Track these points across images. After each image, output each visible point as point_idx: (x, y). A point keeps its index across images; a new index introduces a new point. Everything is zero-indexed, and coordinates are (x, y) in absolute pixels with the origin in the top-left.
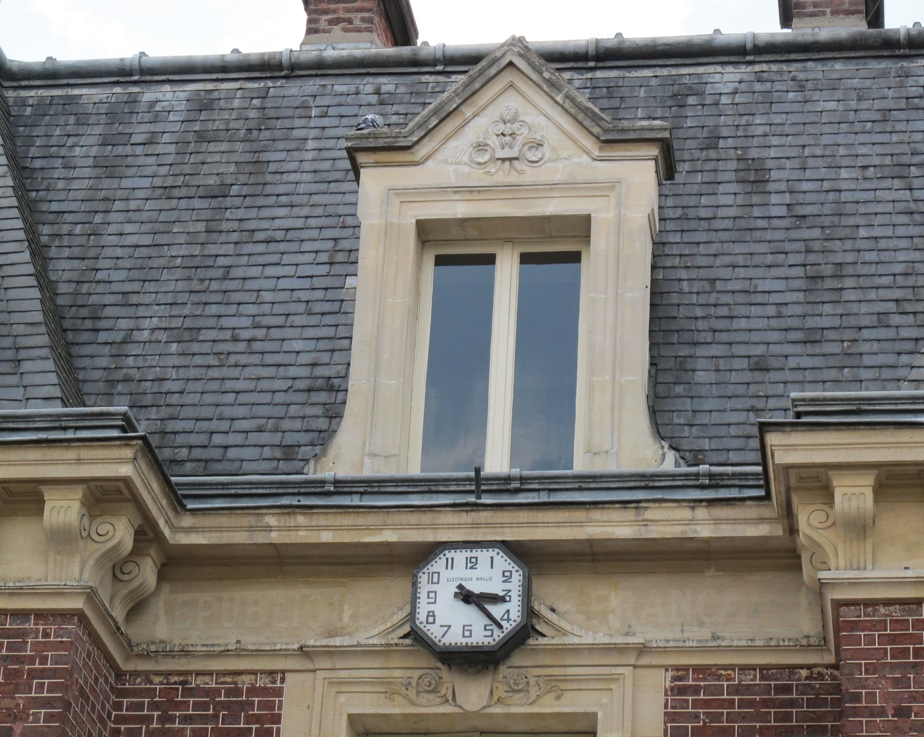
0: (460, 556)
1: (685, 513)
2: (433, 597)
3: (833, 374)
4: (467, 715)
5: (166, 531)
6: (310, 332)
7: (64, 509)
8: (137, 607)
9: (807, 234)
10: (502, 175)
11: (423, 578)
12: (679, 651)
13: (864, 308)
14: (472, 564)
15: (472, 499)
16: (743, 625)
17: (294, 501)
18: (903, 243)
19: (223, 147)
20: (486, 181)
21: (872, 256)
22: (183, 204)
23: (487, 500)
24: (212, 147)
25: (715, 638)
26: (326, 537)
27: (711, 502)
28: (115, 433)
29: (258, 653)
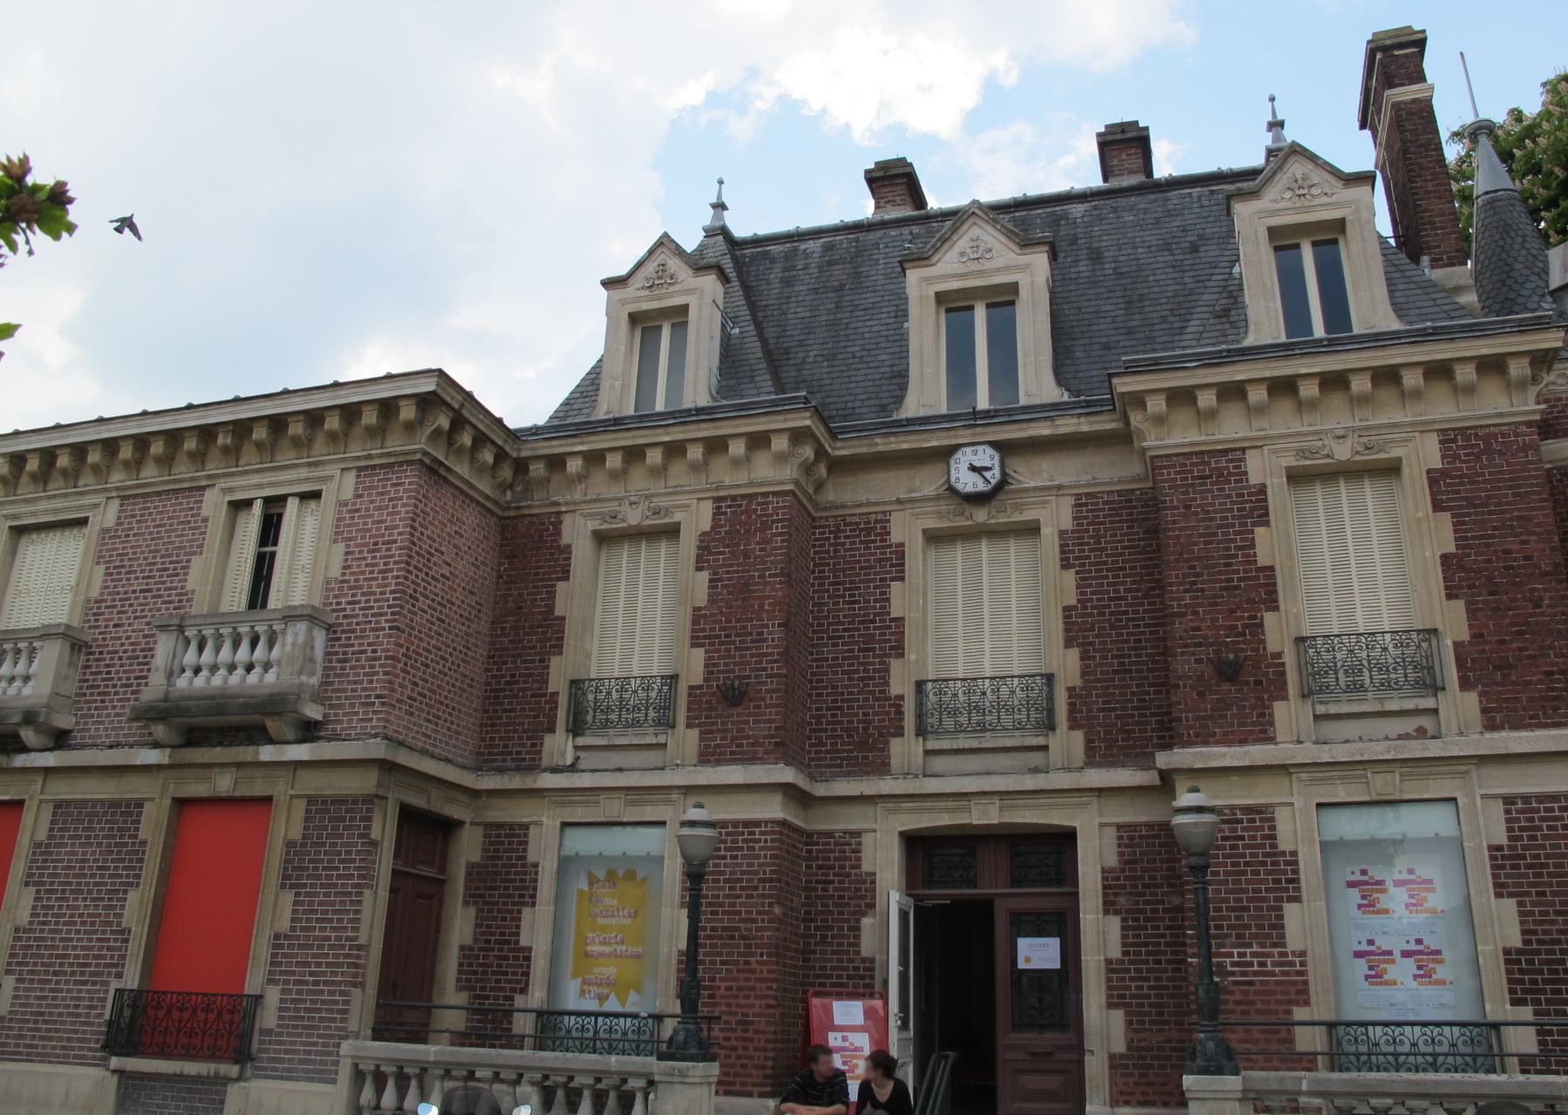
0: (969, 450)
4: (978, 525)
7: (780, 444)
8: (819, 486)
10: (974, 267)
20: (966, 270)
26: (905, 446)
27: (1087, 414)
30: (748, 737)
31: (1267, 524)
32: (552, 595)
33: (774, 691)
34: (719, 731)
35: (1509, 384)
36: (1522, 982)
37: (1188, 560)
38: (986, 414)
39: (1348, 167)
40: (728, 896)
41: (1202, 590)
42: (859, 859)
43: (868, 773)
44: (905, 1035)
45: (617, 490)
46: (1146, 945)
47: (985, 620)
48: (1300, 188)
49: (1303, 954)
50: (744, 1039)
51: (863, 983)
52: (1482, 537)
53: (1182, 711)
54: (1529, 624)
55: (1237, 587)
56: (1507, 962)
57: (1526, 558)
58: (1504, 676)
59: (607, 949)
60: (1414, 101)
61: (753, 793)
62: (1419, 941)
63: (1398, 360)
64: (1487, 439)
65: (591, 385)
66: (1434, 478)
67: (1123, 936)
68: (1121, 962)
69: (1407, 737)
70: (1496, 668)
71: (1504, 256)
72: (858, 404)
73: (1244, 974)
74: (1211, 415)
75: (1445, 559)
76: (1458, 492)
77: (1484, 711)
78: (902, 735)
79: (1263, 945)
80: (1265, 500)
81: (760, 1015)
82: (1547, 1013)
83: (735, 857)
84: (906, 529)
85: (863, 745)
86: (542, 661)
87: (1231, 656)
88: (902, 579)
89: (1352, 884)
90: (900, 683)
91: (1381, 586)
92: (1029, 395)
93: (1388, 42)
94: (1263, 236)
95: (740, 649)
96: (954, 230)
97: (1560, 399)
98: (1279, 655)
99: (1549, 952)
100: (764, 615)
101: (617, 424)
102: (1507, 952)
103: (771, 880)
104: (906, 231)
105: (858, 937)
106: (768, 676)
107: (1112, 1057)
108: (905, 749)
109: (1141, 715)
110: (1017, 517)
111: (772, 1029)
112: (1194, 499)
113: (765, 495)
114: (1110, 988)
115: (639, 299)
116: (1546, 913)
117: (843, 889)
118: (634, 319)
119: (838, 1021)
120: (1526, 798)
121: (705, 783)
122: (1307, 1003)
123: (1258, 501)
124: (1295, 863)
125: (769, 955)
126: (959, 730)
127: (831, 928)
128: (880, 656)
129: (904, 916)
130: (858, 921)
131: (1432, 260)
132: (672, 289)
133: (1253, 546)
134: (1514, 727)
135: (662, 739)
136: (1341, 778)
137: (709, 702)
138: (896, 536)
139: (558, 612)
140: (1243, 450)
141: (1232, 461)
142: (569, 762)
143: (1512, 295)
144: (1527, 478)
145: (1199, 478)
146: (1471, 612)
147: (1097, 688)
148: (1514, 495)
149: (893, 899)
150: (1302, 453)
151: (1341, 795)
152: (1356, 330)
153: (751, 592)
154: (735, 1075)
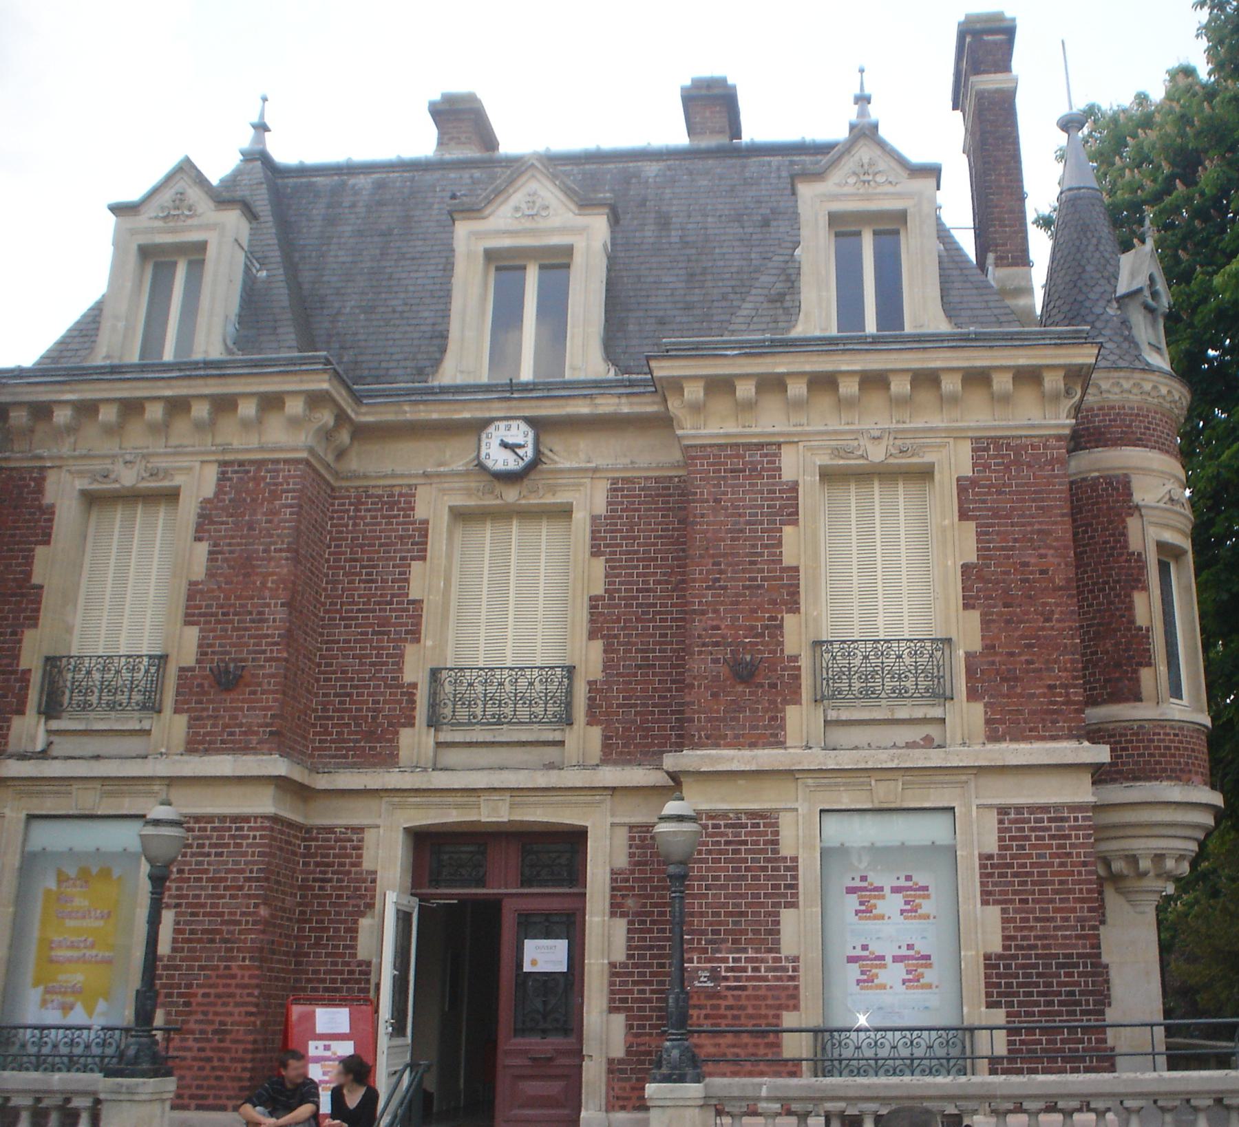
0: (502, 425)
1: (616, 400)
2: (488, 445)
3: (697, 326)
4: (508, 504)
5: (353, 416)
6: (433, 307)
7: (295, 407)
8: (341, 454)
9: (688, 252)
10: (528, 224)
11: (484, 436)
12: (613, 470)
13: (716, 291)
14: (509, 428)
15: (508, 395)
16: (643, 457)
17: (419, 398)
18: (737, 256)
19: (391, 208)
20: (520, 227)
21: (722, 263)
22: (369, 239)
23: (515, 396)
24: (385, 208)
25: (632, 463)
26: (435, 416)
27: (628, 395)
28: (320, 367)
29: (402, 476)
30: (241, 725)
31: (795, 523)
32: (29, 560)
33: (272, 676)
34: (209, 717)
35: (1043, 396)
36: (999, 985)
37: (713, 556)
38: (525, 387)
39: (916, 157)
40: (211, 897)
41: (725, 588)
42: (360, 856)
43: (374, 765)
44: (399, 1041)
45: (109, 446)
46: (651, 948)
47: (509, 608)
48: (865, 173)
49: (796, 959)
50: (220, 1050)
51: (353, 988)
52: (1003, 549)
53: (695, 712)
54: (1038, 638)
55: (759, 587)
56: (987, 967)
57: (1042, 572)
58: (1009, 688)
59: (74, 954)
60: (997, 91)
61: (242, 784)
62: (910, 947)
63: (938, 364)
64: (1018, 450)
65: (88, 328)
66: (964, 486)
67: (629, 939)
68: (625, 965)
69: (910, 745)
70: (1003, 680)
71: (1079, 256)
72: (393, 364)
73: (737, 979)
74: (748, 406)
75: (966, 568)
76: (984, 502)
77: (988, 722)
78: (413, 725)
79: (757, 951)
80: (797, 498)
81: (239, 1024)
82: (1018, 1014)
83: (221, 854)
84: (431, 506)
85: (370, 735)
86: (14, 633)
87: (748, 658)
88: (424, 558)
89: (851, 890)
90: (414, 671)
91: (905, 591)
92: (573, 368)
93: (978, 26)
94: (823, 221)
95: (238, 629)
96: (511, 182)
97: (1113, 408)
98: (795, 658)
99: (1026, 957)
100: (267, 593)
101: (115, 372)
102: (987, 957)
103: (257, 880)
104: (466, 175)
105: (354, 939)
106: (266, 660)
107: (610, 1061)
108: (415, 741)
109: (660, 713)
110: (549, 499)
111: (251, 1038)
112: (725, 493)
113: (277, 461)
114: (612, 992)
115: (152, 230)
116: (1027, 920)
117: (341, 888)
118: (146, 252)
119: (320, 1029)
120: (1019, 809)
121: (190, 774)
122: (796, 1008)
123: (788, 499)
124: (796, 868)
125: (251, 959)
127: (327, 929)
128: (394, 640)
129: (403, 918)
130: (356, 922)
131: (997, 258)
132: (189, 222)
133: (780, 545)
134: (1014, 739)
135: (146, 725)
136: (845, 784)
137: (201, 686)
138: (420, 512)
139: (35, 580)
140: (779, 445)
141: (766, 455)
142: (39, 748)
143: (1080, 298)
144: (1052, 492)
145: (732, 471)
146: (986, 623)
147: (618, 683)
148: (1038, 508)
149: (392, 897)
150: (837, 452)
151: (846, 802)
152: (908, 329)
153: (254, 567)
154: (209, 1088)
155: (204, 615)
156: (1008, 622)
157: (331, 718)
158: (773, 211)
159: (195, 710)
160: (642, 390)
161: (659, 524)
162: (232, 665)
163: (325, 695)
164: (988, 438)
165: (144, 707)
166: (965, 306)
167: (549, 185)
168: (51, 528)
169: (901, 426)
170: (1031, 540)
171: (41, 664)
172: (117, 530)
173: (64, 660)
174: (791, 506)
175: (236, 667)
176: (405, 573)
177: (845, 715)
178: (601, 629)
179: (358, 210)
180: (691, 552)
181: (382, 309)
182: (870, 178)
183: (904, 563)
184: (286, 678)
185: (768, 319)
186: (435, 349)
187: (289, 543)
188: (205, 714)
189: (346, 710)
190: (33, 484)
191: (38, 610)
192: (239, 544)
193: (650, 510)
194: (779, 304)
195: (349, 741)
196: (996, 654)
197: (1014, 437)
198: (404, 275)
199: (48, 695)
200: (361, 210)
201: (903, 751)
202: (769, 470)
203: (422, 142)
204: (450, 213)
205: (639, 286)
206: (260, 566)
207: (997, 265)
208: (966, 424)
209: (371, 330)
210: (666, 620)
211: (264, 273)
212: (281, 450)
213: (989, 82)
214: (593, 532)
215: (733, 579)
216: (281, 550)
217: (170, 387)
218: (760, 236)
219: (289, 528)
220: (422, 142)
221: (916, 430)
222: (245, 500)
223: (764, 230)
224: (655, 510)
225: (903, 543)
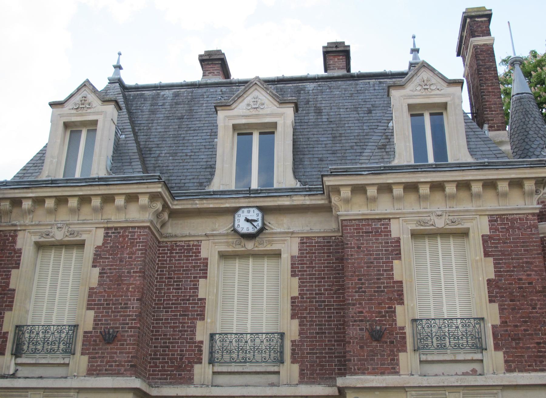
0: (246, 210)
1: (303, 198)
3: (339, 162)
5: (170, 205)
6: (206, 153)
7: (144, 200)
8: (163, 225)
10: (254, 112)
11: (236, 216)
12: (302, 233)
14: (249, 212)
15: (248, 195)
16: (317, 226)
18: (357, 128)
19: (182, 106)
20: (250, 114)
21: (349, 131)
22: (172, 121)
23: (252, 195)
25: (311, 229)
26: (211, 206)
27: (309, 195)
28: (157, 180)
29: (194, 236)
30: (116, 361)
33: (132, 336)
37: (358, 276)
38: (256, 191)
41: (365, 292)
43: (181, 383)
45: (50, 220)
48: (425, 85)
52: (508, 271)
53: (351, 356)
54: (529, 317)
57: (529, 283)
58: (516, 344)
64: (513, 221)
66: (486, 239)
71: (525, 127)
74: (374, 200)
75: (489, 281)
76: (497, 247)
77: (506, 362)
78: (201, 363)
80: (399, 246)
84: (209, 251)
88: (206, 277)
90: (201, 334)
92: (279, 183)
94: (406, 108)
98: (403, 328)
100: (129, 294)
101: (53, 183)
104: (219, 89)
106: (129, 328)
110: (269, 248)
112: (363, 244)
118: (66, 125)
121: (90, 386)
123: (395, 246)
126: (232, 361)
128: (191, 319)
132: (89, 111)
133: (392, 270)
134: (521, 371)
135: (66, 361)
137: (95, 341)
138: (203, 255)
139: (11, 286)
140: (389, 219)
141: (383, 225)
142: (11, 372)
143: (528, 147)
145: (366, 232)
146: (501, 310)
147: (307, 342)
148: (525, 250)
150: (419, 223)
152: (450, 160)
153: (122, 280)
155: (98, 305)
156: (513, 309)
157: (159, 359)
158: (373, 106)
159: (92, 353)
160: (315, 193)
161: (326, 260)
162: (111, 331)
163: (155, 347)
164: (496, 215)
165: (65, 351)
166: (478, 150)
167: (264, 93)
168: (20, 260)
169: (452, 209)
170: (523, 267)
171: (13, 329)
172: (52, 262)
173: (25, 327)
174: (397, 250)
175: (114, 332)
176: (196, 285)
177: (430, 358)
178: (297, 314)
179: (166, 107)
180: (347, 274)
181: (181, 154)
182: (428, 87)
183: (455, 279)
184: (139, 337)
185: (379, 157)
186: (208, 173)
187: (140, 269)
188: (97, 356)
189: (166, 355)
190: (11, 238)
191: (12, 302)
192: (115, 269)
193: (321, 253)
194: (383, 150)
195: (168, 370)
196: (508, 326)
197: (510, 214)
198: (191, 138)
199: (17, 345)
200: (167, 106)
201: (461, 377)
202: (385, 232)
203: (195, 74)
204: (215, 107)
205: (308, 143)
206: (125, 280)
207: (489, 130)
208: (486, 208)
209: (176, 164)
210: (331, 309)
211: (124, 136)
212: (137, 222)
213: (480, 41)
214: (292, 264)
215: (368, 287)
216: (136, 272)
217: (82, 191)
218: (367, 118)
219: (140, 261)
220: (195, 74)
221: (460, 211)
222: (118, 247)
223: (369, 115)
224: (323, 253)
225: (454, 269)
